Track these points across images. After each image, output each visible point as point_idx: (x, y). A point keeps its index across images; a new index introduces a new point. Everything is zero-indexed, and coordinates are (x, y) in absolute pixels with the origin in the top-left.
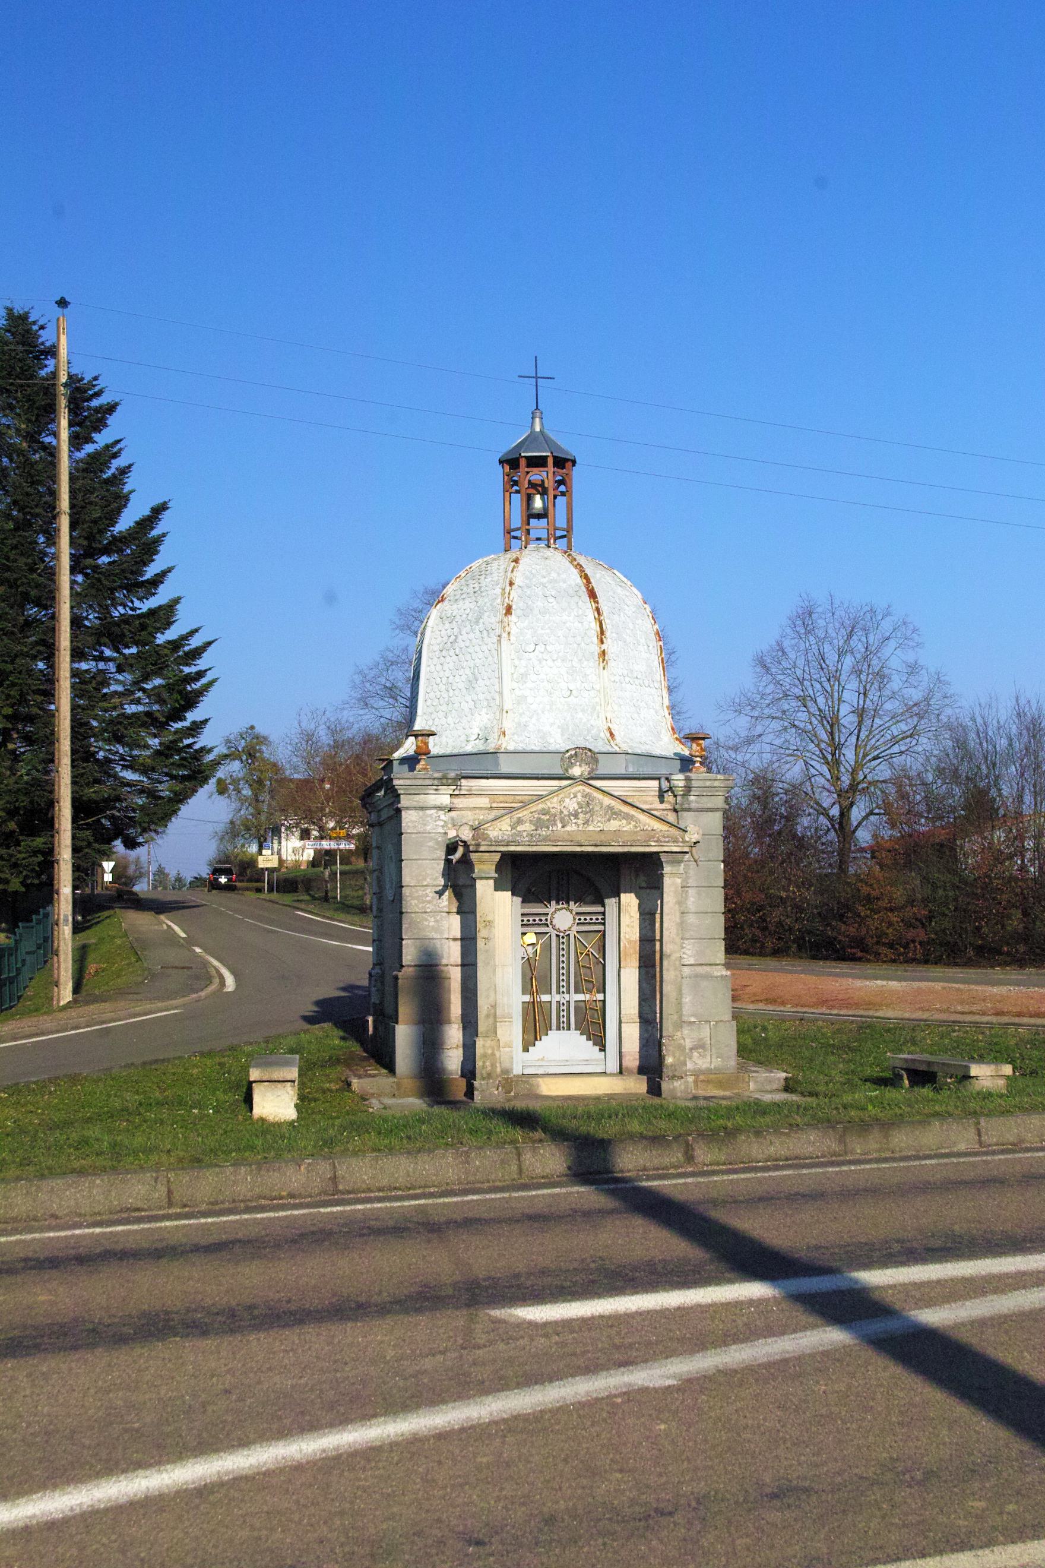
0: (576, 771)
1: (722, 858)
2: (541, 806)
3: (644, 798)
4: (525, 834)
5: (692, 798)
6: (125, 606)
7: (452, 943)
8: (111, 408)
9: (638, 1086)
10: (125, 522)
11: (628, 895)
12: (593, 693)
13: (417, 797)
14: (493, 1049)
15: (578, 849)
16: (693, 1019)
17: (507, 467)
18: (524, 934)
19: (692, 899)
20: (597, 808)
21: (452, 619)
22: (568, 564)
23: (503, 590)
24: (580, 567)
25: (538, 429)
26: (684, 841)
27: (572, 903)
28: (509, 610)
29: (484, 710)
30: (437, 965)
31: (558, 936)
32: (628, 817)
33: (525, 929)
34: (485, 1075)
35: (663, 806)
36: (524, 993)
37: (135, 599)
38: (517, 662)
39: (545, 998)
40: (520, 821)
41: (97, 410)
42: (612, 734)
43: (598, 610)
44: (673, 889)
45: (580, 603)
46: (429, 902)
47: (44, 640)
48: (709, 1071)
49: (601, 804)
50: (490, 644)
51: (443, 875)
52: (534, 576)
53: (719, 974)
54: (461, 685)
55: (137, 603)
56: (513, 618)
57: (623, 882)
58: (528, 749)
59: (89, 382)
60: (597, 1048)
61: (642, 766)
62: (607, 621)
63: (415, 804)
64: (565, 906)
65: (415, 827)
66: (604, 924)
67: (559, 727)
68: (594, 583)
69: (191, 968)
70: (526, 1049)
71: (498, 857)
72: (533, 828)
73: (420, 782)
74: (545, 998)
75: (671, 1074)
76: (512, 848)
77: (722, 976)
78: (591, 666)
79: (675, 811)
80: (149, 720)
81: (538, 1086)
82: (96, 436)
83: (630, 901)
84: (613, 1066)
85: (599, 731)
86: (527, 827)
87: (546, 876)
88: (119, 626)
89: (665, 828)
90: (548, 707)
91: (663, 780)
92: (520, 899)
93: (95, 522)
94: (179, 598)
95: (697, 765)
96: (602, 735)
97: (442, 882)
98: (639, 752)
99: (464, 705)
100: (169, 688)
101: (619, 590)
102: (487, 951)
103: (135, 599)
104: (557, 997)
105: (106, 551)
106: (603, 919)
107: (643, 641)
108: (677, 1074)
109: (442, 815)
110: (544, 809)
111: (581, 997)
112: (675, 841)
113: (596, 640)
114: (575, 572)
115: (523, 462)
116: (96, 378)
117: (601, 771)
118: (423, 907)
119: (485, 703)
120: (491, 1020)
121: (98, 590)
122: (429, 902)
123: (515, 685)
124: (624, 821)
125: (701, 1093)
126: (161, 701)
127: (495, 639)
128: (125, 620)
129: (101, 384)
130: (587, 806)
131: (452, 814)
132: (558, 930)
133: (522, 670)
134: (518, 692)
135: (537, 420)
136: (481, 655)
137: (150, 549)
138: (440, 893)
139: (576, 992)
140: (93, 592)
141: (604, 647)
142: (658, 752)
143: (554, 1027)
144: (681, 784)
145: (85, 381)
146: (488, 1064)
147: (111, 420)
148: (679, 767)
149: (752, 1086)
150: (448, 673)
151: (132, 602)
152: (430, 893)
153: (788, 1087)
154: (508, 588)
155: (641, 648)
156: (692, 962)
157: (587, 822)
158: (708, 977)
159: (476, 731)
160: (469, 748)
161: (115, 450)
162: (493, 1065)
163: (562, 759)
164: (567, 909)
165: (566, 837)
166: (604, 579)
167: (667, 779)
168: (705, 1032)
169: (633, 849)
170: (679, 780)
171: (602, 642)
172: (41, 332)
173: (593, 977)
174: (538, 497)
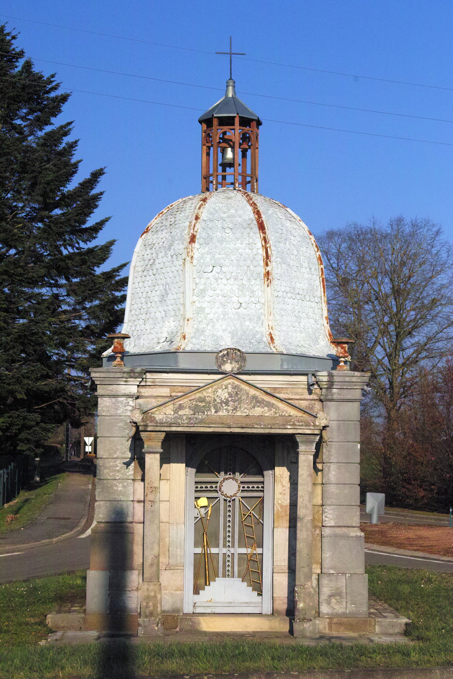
0: (228, 367)
1: (358, 440)
2: (198, 395)
3: (294, 390)
4: (185, 417)
5: (335, 391)
6: (73, 246)
7: (136, 504)
8: (64, 98)
9: (281, 626)
10: (72, 185)
11: (281, 468)
12: (258, 306)
13: (111, 387)
14: (155, 592)
15: (228, 430)
16: (332, 572)
17: (205, 126)
18: (197, 498)
19: (333, 473)
20: (244, 397)
21: (152, 246)
22: (245, 202)
23: (190, 223)
24: (254, 205)
25: (230, 95)
26: (315, 425)
27: (237, 474)
28: (193, 239)
29: (172, 319)
30: (123, 522)
31: (225, 500)
32: (269, 405)
33: (198, 495)
34: (148, 613)
35: (311, 397)
36: (196, 545)
37: (80, 242)
38: (197, 280)
39: (214, 550)
40: (181, 407)
41: (54, 100)
42: (272, 339)
43: (265, 239)
44: (306, 464)
45: (251, 234)
46: (119, 471)
47: (6, 271)
48: (344, 615)
49: (248, 394)
50: (178, 266)
51: (130, 450)
52: (217, 211)
53: (354, 535)
54: (157, 299)
55: (82, 245)
56: (196, 245)
57: (276, 458)
58: (202, 349)
59: (48, 78)
60: (256, 593)
61: (296, 365)
62: (273, 248)
63: (109, 393)
64: (232, 476)
65: (108, 411)
66: (263, 491)
67: (230, 333)
68: (264, 217)
69: (70, 519)
70: (196, 591)
71: (163, 435)
72: (192, 412)
73: (112, 375)
74: (214, 550)
75: (302, 617)
76: (174, 429)
77: (357, 536)
78: (258, 285)
79: (321, 400)
80: (88, 332)
81: (199, 624)
82: (53, 120)
83: (282, 472)
84: (267, 609)
85: (262, 336)
86: (186, 412)
87: (217, 452)
88: (64, 261)
89: (300, 414)
90: (222, 316)
91: (310, 375)
92: (194, 470)
93: (48, 183)
94: (114, 241)
95: (342, 364)
96: (265, 339)
97: (129, 455)
98: (294, 353)
99: (158, 315)
100: (101, 307)
101: (288, 224)
102: (152, 512)
103: (80, 242)
104: (225, 550)
105: (57, 205)
106: (263, 487)
107: (306, 265)
108: (307, 617)
109: (131, 402)
110: (200, 397)
111: (243, 550)
112: (308, 425)
113: (262, 263)
114: (250, 208)
115: (215, 122)
116: (53, 76)
117: (249, 367)
118: (114, 475)
119: (173, 313)
120: (154, 568)
121: (49, 234)
122: (119, 471)
123: (195, 298)
124: (266, 408)
125: (335, 634)
126: (97, 318)
127: (181, 262)
128: (70, 257)
129: (57, 80)
130: (236, 396)
131: (140, 401)
132: (226, 496)
133: (202, 287)
134: (197, 304)
135: (230, 88)
136: (171, 274)
137: (90, 204)
138: (127, 464)
139: (240, 546)
140: (45, 235)
141: (268, 268)
142: (312, 353)
143: (220, 574)
144: (325, 379)
145: (45, 78)
146: (151, 604)
147: (65, 107)
148: (332, 366)
149: (377, 629)
150: (147, 289)
151: (78, 243)
152: (119, 464)
153: (407, 631)
154: (194, 221)
155: (303, 270)
156: (333, 524)
157: (235, 409)
158: (346, 537)
159: (165, 335)
160: (158, 349)
161: (66, 130)
162: (155, 606)
163: (217, 358)
164: (233, 479)
165: (218, 421)
166: (273, 214)
167: (313, 375)
168: (342, 582)
169: (192, 429)
170: (323, 376)
171: (267, 265)
172: (13, 41)
173: (253, 534)
174: (229, 150)
